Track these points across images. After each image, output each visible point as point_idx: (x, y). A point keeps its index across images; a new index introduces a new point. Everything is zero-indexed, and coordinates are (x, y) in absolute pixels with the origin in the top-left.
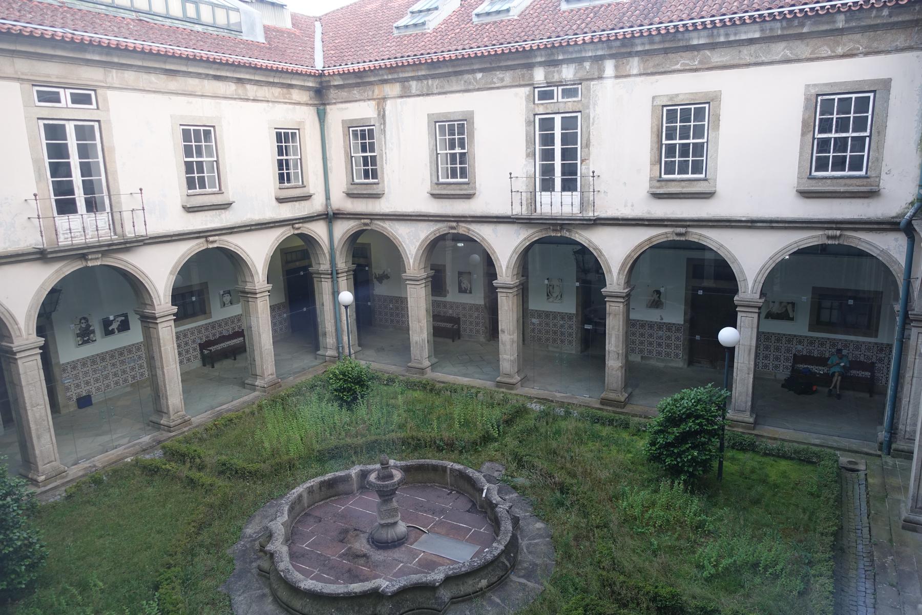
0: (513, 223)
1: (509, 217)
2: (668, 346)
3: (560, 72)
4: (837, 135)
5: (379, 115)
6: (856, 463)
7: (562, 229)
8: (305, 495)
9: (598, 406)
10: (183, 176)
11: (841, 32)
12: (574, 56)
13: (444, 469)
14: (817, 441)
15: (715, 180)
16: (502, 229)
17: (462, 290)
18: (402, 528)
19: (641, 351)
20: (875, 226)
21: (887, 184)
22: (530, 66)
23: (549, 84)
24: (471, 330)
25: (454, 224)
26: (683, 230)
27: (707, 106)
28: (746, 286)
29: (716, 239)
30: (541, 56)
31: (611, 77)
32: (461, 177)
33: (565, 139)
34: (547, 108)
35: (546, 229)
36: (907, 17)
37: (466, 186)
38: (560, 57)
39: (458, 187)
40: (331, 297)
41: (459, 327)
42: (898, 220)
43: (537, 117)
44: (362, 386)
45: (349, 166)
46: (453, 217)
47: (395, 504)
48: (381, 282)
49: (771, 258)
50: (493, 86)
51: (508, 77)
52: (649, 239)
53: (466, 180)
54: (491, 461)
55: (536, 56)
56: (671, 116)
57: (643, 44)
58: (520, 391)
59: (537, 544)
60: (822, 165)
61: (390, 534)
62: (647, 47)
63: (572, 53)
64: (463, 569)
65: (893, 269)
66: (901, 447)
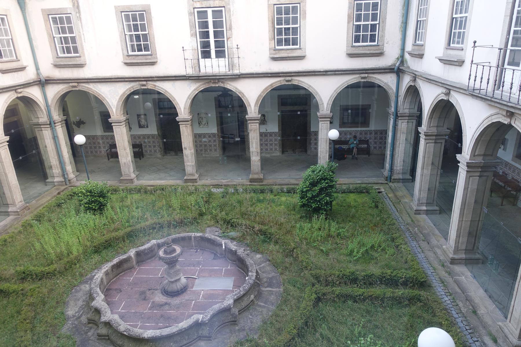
0: (189, 79)
1: (185, 76)
2: (271, 145)
5: (74, 6)
6: (379, 189)
7: (219, 81)
8: (104, 277)
9: (249, 183)
10: (78, 45)
13: (190, 238)
14: (359, 182)
15: (305, 49)
16: (178, 84)
17: (140, 126)
18: (183, 280)
20: (383, 71)
24: (151, 151)
25: (145, 83)
26: (289, 78)
27: (298, 5)
28: (323, 107)
29: (307, 82)
32: (370, 42)
33: (216, 24)
34: (202, 4)
35: (208, 83)
37: (150, 57)
39: (144, 57)
40: (52, 141)
41: (142, 150)
42: (393, 67)
43: (196, 10)
44: (104, 197)
45: (53, 44)
46: (144, 78)
47: (178, 267)
48: (79, 127)
49: (335, 91)
52: (271, 85)
53: (149, 53)
54: (209, 226)
56: (279, 12)
58: (200, 183)
59: (264, 267)
60: (357, 39)
61: (178, 286)
64: (241, 293)
65: (390, 92)
66: (395, 178)
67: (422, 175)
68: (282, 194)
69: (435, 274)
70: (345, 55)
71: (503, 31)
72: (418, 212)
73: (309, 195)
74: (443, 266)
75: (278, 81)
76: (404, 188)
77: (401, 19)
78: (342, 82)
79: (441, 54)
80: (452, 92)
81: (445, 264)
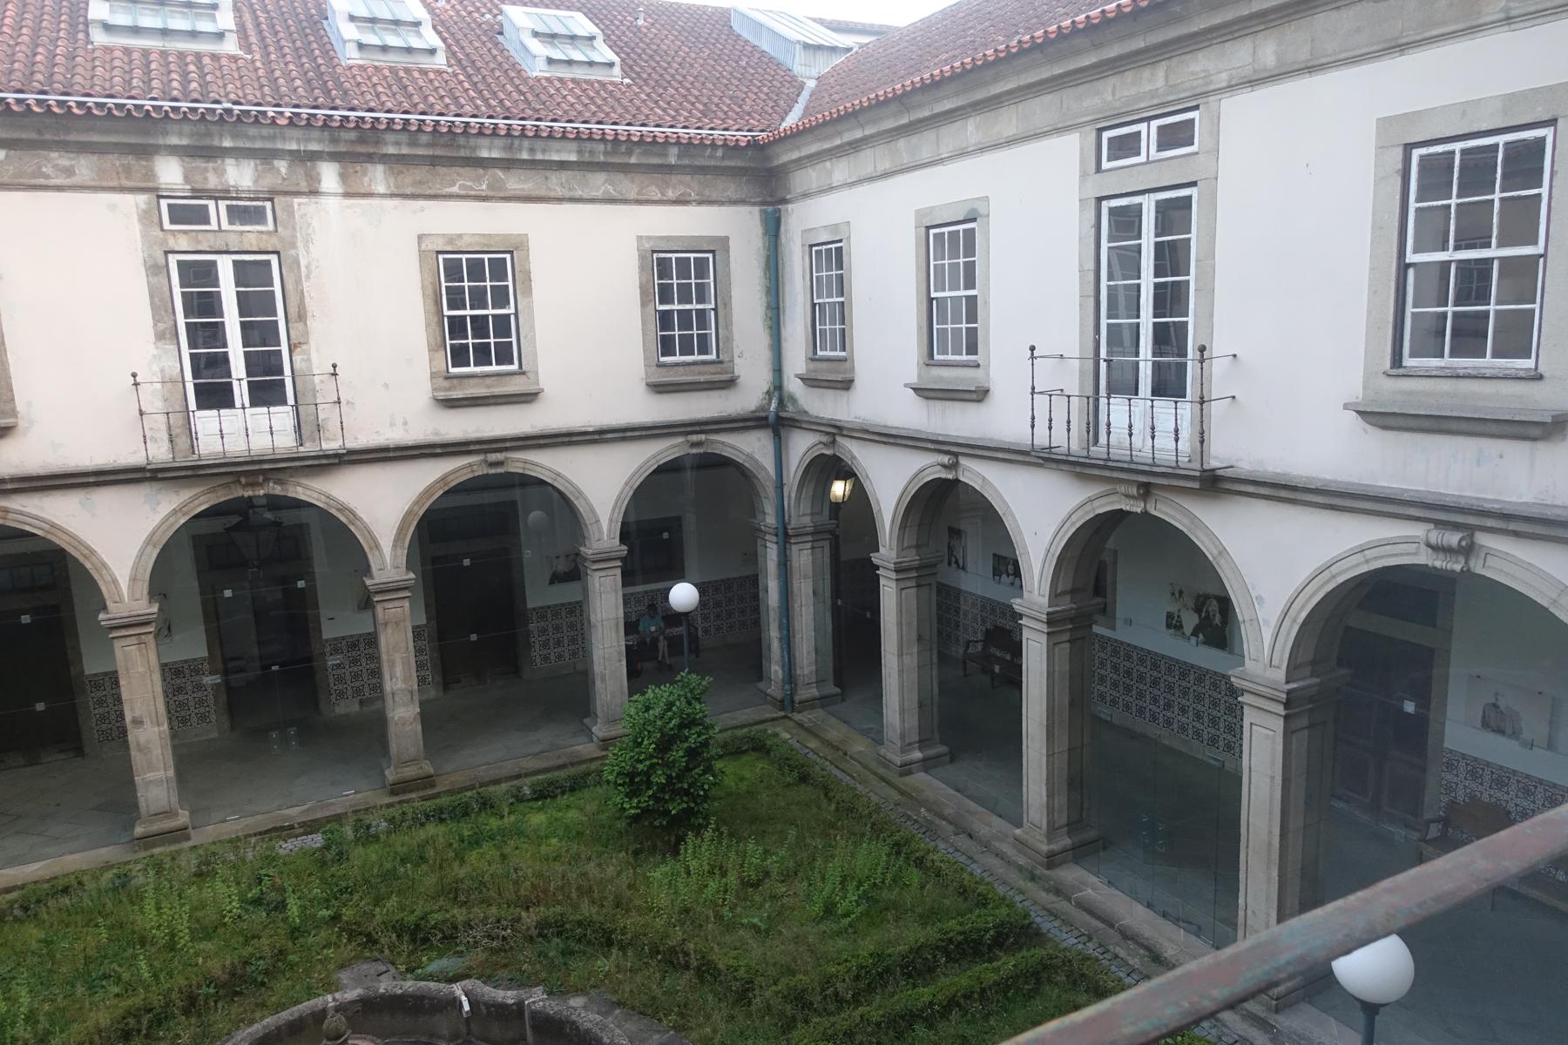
3: (221, 173)
4: (681, 307)
7: (266, 480)
11: (669, 169)
12: (258, 145)
16: (106, 499)
19: (358, 691)
21: (742, 368)
22: (147, 152)
23: (197, 193)
30: (180, 134)
31: (335, 194)
32: (700, 353)
35: (226, 486)
36: (740, 163)
38: (227, 143)
43: (173, 260)
50: (42, 181)
51: (84, 167)
55: (166, 133)
56: (453, 270)
57: (398, 144)
60: (667, 346)
62: (405, 151)
63: (253, 138)
67: (901, 671)
68: (521, 807)
69: (1034, 901)
70: (642, 387)
71: (1081, 325)
72: (906, 769)
73: (659, 778)
74: (1033, 878)
75: (464, 468)
76: (833, 721)
77: (764, 299)
78: (644, 458)
79: (913, 378)
80: (963, 461)
81: (1037, 872)
